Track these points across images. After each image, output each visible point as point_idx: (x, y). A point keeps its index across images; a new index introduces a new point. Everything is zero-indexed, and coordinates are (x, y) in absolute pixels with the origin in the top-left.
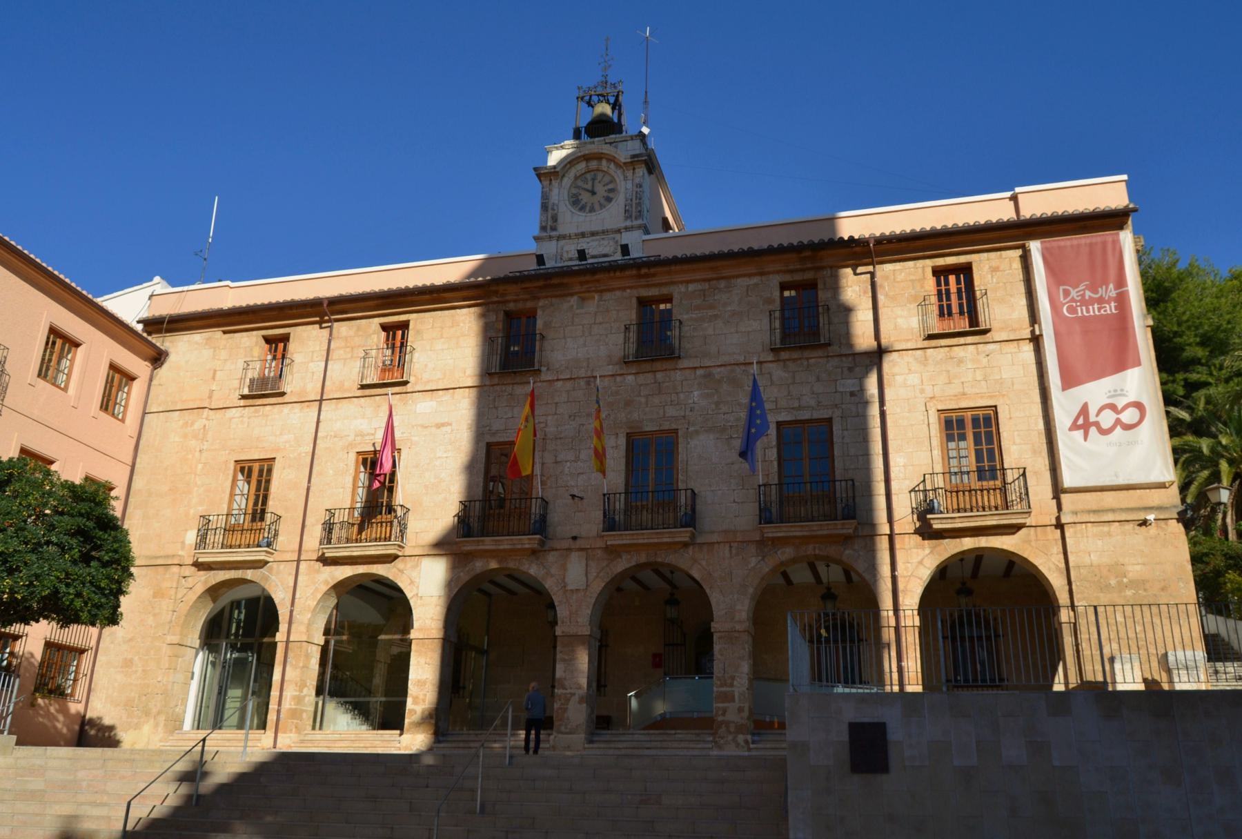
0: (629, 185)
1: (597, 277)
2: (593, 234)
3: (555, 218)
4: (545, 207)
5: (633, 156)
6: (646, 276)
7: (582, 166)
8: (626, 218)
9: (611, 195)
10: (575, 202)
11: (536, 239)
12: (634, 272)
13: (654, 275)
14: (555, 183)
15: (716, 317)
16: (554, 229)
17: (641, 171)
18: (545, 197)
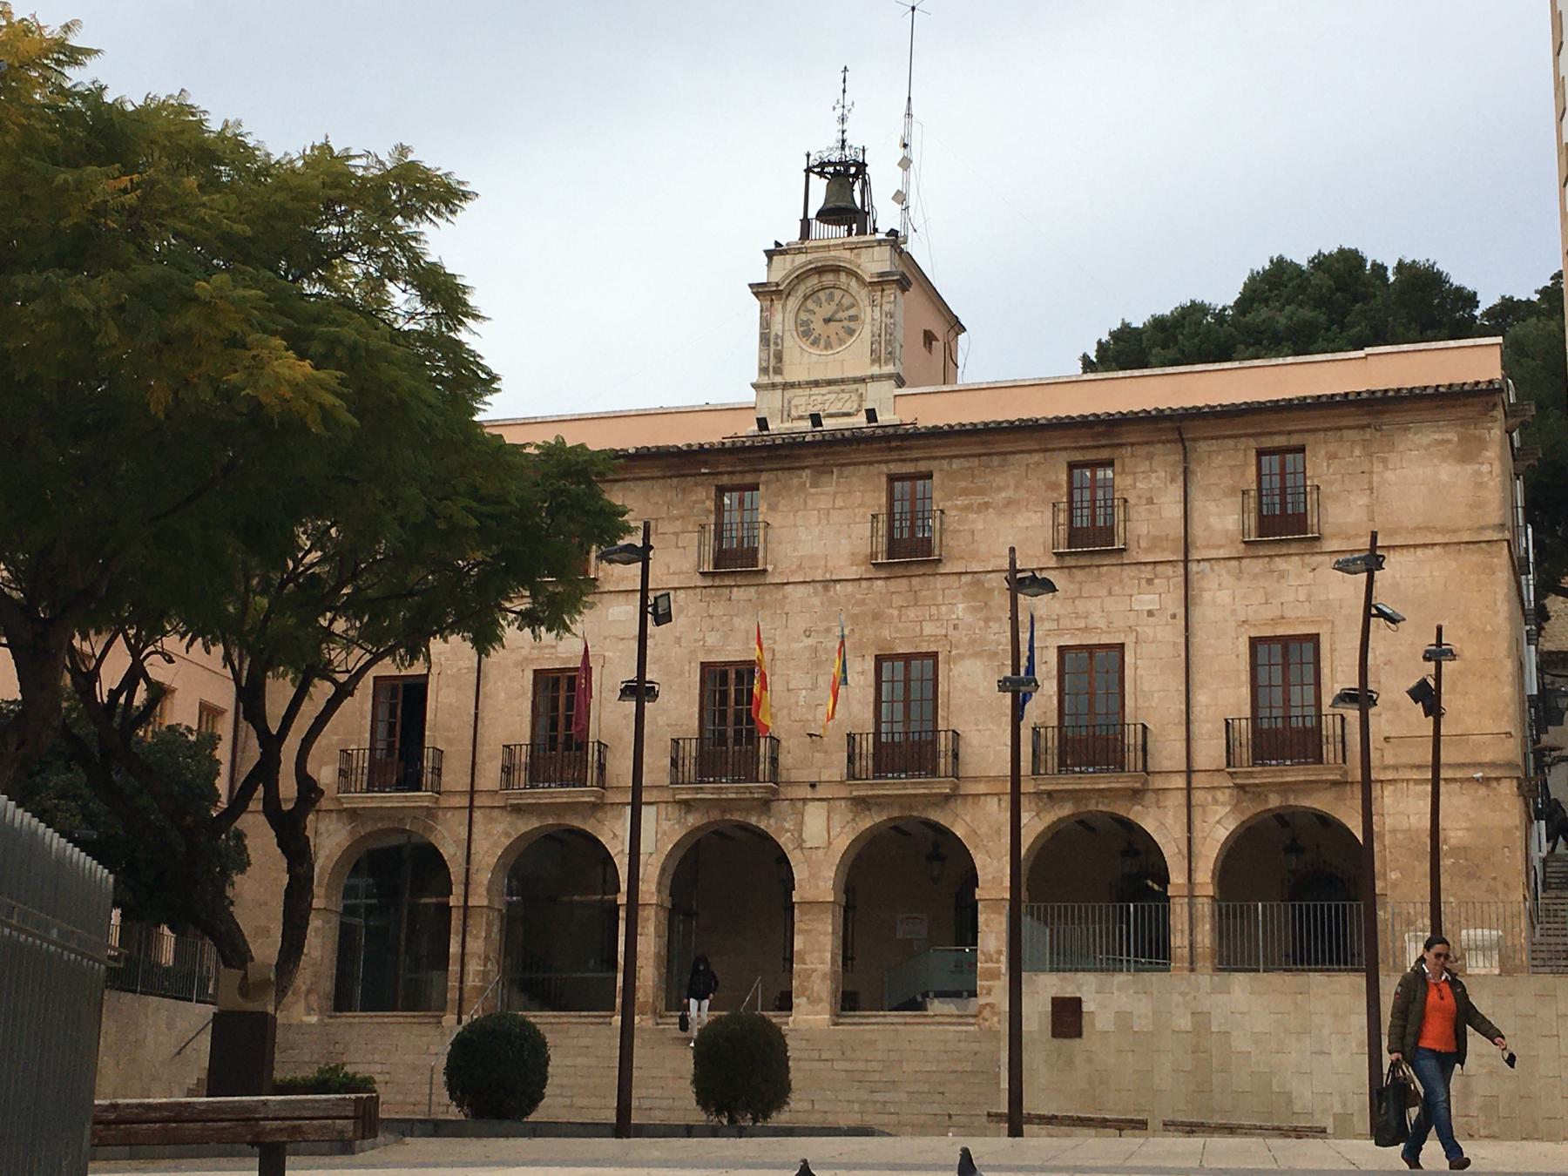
0: (877, 315)
2: (830, 383)
3: (779, 357)
4: (765, 339)
5: (881, 275)
7: (814, 281)
8: (873, 362)
9: (852, 325)
10: (806, 332)
11: (755, 386)
14: (778, 305)
15: (987, 505)
16: (778, 371)
18: (765, 324)
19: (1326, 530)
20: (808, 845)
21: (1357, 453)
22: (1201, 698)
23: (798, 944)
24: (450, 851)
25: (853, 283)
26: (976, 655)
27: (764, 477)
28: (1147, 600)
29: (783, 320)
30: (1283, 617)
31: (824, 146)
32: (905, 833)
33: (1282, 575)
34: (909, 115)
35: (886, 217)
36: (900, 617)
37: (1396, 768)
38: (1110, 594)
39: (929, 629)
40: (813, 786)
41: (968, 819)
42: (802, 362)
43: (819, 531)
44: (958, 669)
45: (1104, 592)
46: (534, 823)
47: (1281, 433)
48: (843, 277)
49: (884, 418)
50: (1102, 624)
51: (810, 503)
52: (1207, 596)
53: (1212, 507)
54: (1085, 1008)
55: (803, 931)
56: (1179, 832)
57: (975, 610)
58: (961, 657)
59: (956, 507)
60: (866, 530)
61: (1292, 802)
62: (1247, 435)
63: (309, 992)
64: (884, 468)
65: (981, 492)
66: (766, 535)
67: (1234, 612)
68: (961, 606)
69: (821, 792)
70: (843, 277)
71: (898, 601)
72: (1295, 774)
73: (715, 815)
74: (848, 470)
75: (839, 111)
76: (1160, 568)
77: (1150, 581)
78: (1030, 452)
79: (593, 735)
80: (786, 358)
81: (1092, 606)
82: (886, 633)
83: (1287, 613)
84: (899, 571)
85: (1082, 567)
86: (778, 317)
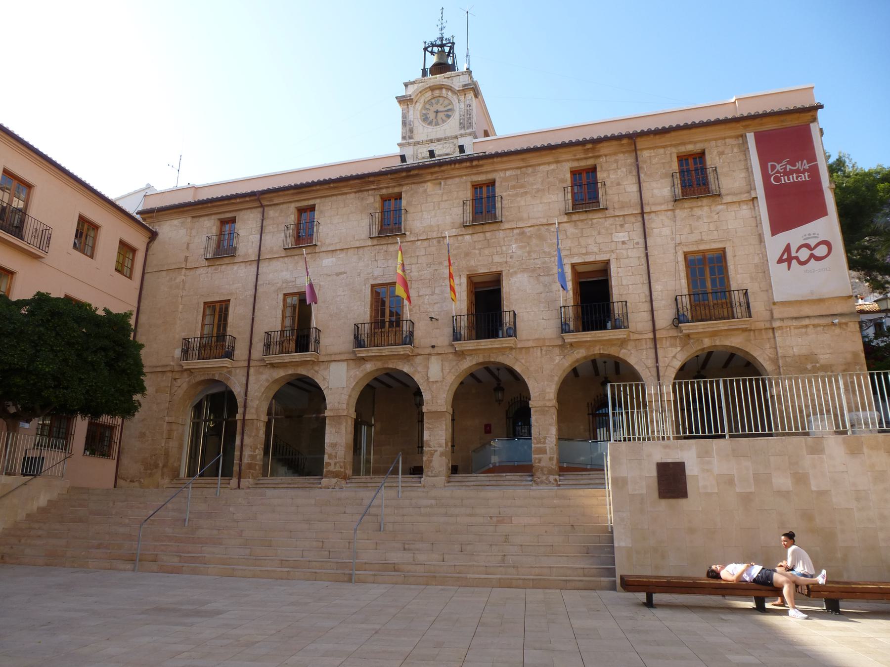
0: (462, 105)
1: (443, 168)
3: (411, 131)
4: (404, 123)
6: (477, 166)
8: (461, 128)
9: (449, 113)
10: (425, 119)
11: (400, 145)
12: (468, 164)
13: (482, 166)
15: (526, 193)
17: (471, 95)
19: (723, 192)
20: (431, 380)
21: (735, 150)
22: (657, 287)
23: (426, 436)
24: (238, 390)
25: (450, 93)
26: (524, 271)
27: (404, 188)
28: (621, 236)
29: (415, 113)
30: (702, 240)
31: (433, 37)
32: (479, 381)
33: (699, 218)
34: (468, 55)
35: (462, 66)
36: (480, 254)
37: (782, 319)
38: (599, 233)
39: (497, 259)
40: (433, 347)
41: (523, 361)
42: (423, 132)
43: (436, 211)
44: (513, 280)
45: (595, 233)
46: (281, 373)
47: (690, 143)
48: (444, 91)
49: (469, 151)
50: (596, 250)
51: (429, 199)
52: (656, 231)
53: (654, 185)
54: (688, 472)
55: (429, 428)
56: (650, 362)
57: (521, 248)
58: (515, 273)
59: (509, 195)
60: (459, 210)
61: (718, 343)
62: (671, 145)
63: (164, 466)
64: (469, 179)
65: (522, 186)
66: (406, 217)
67: (673, 239)
68: (514, 246)
69: (436, 350)
70: (444, 91)
71: (478, 246)
72: (721, 325)
73: (379, 365)
74: (450, 182)
75: (440, 26)
76: (627, 218)
77: (622, 226)
78: (549, 163)
79: (314, 324)
80: (415, 131)
81: (590, 241)
82: (472, 263)
83: (705, 238)
84: (478, 229)
85: (582, 221)
86: (411, 112)
